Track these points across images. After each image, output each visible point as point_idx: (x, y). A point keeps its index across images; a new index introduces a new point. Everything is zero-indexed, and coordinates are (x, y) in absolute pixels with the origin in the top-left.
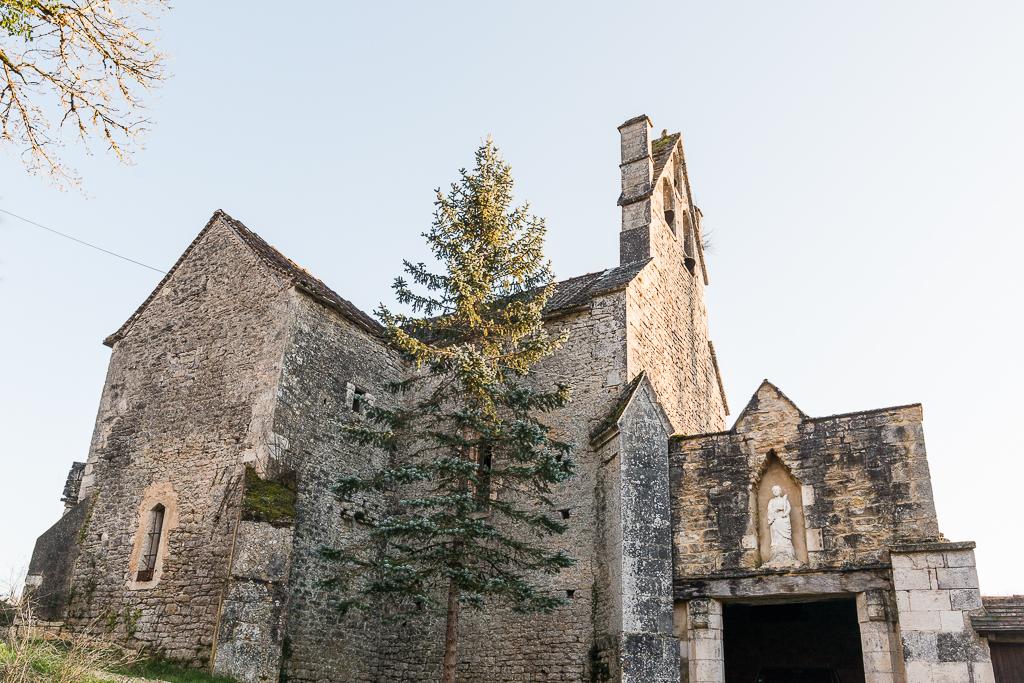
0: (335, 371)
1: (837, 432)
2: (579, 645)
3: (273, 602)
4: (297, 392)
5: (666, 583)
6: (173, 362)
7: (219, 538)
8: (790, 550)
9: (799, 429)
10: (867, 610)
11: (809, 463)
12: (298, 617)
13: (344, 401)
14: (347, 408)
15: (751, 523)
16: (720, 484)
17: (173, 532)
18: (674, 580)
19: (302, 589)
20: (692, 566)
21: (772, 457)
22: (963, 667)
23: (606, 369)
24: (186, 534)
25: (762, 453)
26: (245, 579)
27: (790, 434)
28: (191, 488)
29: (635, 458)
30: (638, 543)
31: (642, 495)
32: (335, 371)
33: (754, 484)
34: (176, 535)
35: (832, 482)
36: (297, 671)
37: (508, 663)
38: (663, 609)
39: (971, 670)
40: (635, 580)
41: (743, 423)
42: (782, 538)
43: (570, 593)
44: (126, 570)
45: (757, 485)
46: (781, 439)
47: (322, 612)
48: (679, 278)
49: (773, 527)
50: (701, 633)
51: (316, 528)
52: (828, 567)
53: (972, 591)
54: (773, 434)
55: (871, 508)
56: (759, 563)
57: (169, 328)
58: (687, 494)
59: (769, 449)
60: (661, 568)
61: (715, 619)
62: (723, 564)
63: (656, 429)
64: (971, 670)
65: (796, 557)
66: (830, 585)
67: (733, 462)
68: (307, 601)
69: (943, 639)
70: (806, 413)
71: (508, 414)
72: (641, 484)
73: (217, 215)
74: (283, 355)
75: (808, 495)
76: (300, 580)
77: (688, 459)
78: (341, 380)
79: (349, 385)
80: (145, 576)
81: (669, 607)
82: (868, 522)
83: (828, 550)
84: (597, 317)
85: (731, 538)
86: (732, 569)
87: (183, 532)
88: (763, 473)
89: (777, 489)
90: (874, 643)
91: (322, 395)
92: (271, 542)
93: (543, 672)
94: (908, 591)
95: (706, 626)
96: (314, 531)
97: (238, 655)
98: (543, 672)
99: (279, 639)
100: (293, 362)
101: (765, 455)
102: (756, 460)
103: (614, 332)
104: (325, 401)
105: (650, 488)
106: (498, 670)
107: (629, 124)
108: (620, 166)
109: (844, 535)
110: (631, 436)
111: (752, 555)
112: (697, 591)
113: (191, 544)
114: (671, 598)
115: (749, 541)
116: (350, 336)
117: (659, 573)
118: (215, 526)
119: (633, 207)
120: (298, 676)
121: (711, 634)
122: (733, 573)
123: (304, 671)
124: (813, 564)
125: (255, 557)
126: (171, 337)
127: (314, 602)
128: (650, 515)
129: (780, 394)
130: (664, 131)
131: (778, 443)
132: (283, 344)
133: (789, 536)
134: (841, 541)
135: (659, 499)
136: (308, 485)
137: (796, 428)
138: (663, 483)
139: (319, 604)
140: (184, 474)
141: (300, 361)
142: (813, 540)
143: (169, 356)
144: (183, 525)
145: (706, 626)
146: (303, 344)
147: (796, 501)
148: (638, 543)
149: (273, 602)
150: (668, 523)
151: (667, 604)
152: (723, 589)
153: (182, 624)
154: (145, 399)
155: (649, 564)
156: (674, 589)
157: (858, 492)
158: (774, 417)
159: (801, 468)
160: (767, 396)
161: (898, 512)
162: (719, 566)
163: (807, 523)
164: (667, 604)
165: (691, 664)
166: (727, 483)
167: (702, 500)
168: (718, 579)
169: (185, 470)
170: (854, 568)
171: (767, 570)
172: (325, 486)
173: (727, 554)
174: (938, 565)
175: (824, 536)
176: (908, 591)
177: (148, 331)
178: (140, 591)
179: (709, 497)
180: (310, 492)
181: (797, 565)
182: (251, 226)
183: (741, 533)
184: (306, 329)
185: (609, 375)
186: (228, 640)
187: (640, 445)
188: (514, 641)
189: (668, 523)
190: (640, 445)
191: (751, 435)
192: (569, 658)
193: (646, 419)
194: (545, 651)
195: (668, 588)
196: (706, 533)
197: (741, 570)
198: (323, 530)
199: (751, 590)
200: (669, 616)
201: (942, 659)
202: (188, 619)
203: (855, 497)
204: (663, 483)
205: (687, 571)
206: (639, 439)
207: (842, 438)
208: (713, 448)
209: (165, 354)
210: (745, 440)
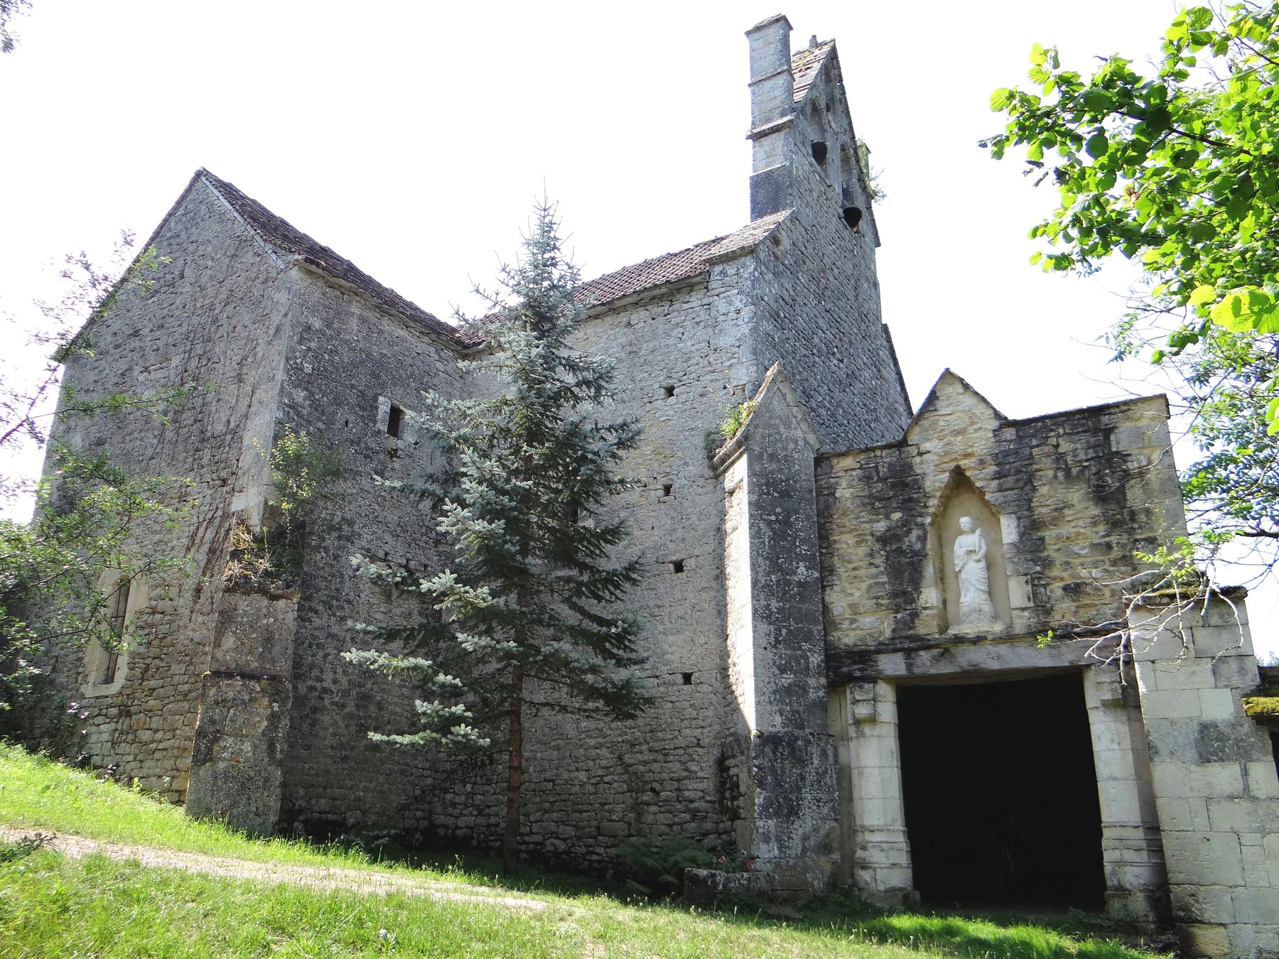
0: (362, 380)
2: (700, 751)
3: (270, 706)
4: (305, 412)
5: (816, 659)
6: (141, 378)
7: (200, 619)
8: (987, 607)
9: (995, 436)
10: (1096, 693)
12: (313, 725)
13: (375, 422)
14: (379, 432)
15: (929, 570)
16: (887, 517)
17: (141, 613)
18: (826, 656)
19: (318, 685)
20: (852, 634)
21: (958, 473)
22: (1234, 769)
23: (728, 363)
24: (158, 616)
26: (230, 675)
27: (982, 441)
28: (164, 551)
29: (767, 484)
30: (775, 604)
31: (778, 536)
32: (362, 380)
34: (145, 617)
35: (1043, 510)
36: (314, 801)
37: (606, 779)
38: (812, 695)
39: (1245, 773)
40: (771, 655)
42: (976, 589)
43: (687, 678)
44: (81, 670)
46: (970, 451)
47: (350, 716)
48: (836, 236)
49: (963, 575)
50: (867, 729)
51: (338, 600)
53: (1244, 656)
54: (959, 443)
56: (944, 628)
57: (136, 334)
58: (841, 533)
59: (953, 465)
60: (808, 637)
61: (888, 711)
62: (894, 631)
63: (796, 442)
64: (1245, 773)
65: (995, 617)
66: (1041, 656)
68: (327, 702)
69: (1206, 729)
72: (777, 521)
73: (198, 175)
74: (283, 360)
75: (1009, 530)
76: (315, 672)
78: (370, 393)
79: (381, 399)
80: (109, 679)
81: (821, 693)
82: (1095, 565)
83: (1042, 607)
84: (716, 292)
85: (905, 593)
86: (907, 637)
87: (154, 613)
88: (946, 503)
89: (965, 521)
90: (1108, 740)
91: (342, 414)
92: (265, 621)
93: (653, 790)
94: (1153, 662)
95: (873, 720)
96: (335, 603)
97: (220, 783)
98: (653, 790)
99: (279, 756)
100: (299, 369)
101: (947, 474)
102: (935, 480)
103: (738, 312)
104: (347, 423)
105: (790, 525)
106: (592, 789)
107: (758, 29)
108: (750, 85)
109: (1062, 584)
110: (761, 454)
112: (860, 670)
113: (165, 628)
114: (823, 680)
115: (929, 596)
116: (381, 332)
117: (805, 646)
118: (195, 603)
119: (766, 141)
120: (316, 809)
121: (879, 730)
122: (908, 643)
123: (323, 801)
124: (1020, 626)
125: (243, 644)
126: (137, 344)
127: (336, 704)
128: (791, 564)
129: (966, 387)
130: (814, 37)
131: (967, 455)
132: (281, 345)
133: (984, 587)
134: (1060, 592)
135: (803, 541)
136: (324, 540)
138: (808, 517)
139: (344, 706)
140: (156, 532)
141: (308, 368)
142: (1017, 593)
143: (137, 369)
144: (154, 603)
145: (873, 720)
146: (313, 345)
147: (993, 538)
148: (775, 604)
149: (270, 706)
150: (816, 575)
151: (818, 688)
152: (892, 664)
153: (152, 742)
154: (106, 434)
155: (790, 632)
156: (828, 668)
157: (1081, 522)
158: (959, 421)
159: (1000, 491)
162: (888, 634)
163: (1010, 569)
164: (818, 688)
165: (855, 772)
166: (897, 516)
167: (863, 541)
169: (157, 527)
172: (348, 539)
173: (899, 616)
174: (1194, 623)
175: (1033, 586)
176: (1153, 662)
177: (109, 338)
178: (97, 698)
179: (872, 535)
180: (326, 550)
181: (998, 628)
182: (250, 190)
184: (317, 324)
185: (733, 371)
186: (205, 761)
187: (774, 466)
188: (612, 747)
189: (816, 575)
190: (774, 466)
192: (687, 770)
193: (782, 430)
194: (655, 761)
195: (819, 666)
196: (870, 587)
197: (918, 638)
198: (349, 602)
199: (926, 663)
200: (822, 706)
201: (1204, 759)
202: (159, 735)
205: (846, 640)
206: (772, 457)
207: (1057, 446)
208: (876, 467)
209: (130, 369)
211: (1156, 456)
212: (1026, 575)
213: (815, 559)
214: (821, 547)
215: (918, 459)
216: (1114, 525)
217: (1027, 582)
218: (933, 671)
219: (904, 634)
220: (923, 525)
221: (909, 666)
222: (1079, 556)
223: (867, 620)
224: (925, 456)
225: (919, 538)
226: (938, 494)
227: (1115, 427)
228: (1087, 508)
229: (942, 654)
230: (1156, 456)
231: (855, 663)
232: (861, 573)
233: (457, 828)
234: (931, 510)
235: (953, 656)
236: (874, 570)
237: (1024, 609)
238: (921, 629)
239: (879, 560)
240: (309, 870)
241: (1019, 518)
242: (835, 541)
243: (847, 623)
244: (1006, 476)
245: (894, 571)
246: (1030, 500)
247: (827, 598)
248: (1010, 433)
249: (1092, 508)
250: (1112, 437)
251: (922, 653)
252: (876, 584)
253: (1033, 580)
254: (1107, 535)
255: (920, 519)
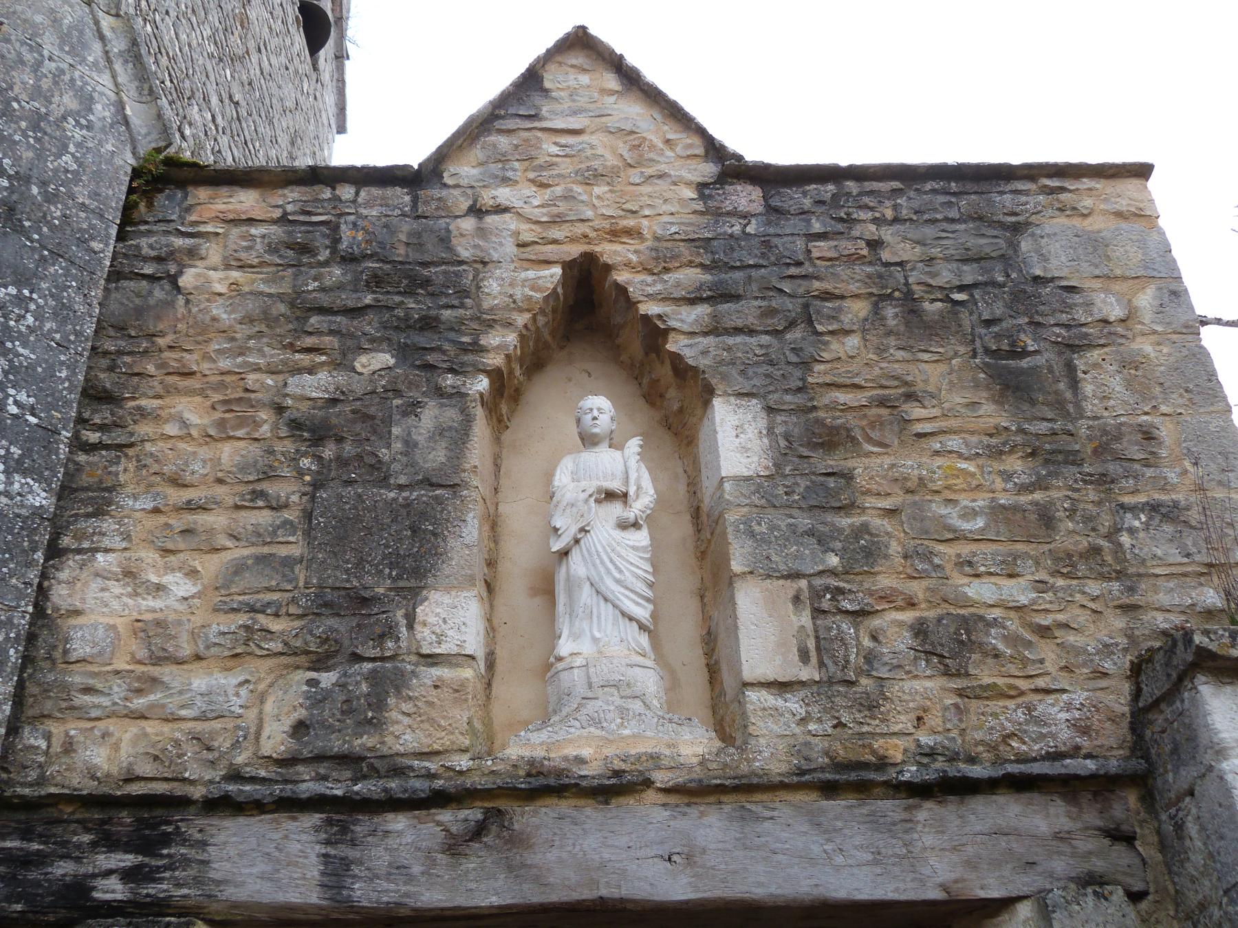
1: (849, 221)
11: (746, 312)
20: (127, 733)
25: (548, 263)
27: (668, 200)
33: (496, 375)
41: (477, 153)
45: (506, 394)
46: (630, 222)
49: (577, 565)
52: (839, 766)
55: (1015, 508)
59: (575, 251)
62: (300, 728)
63: (87, 102)
67: (416, 284)
70: (733, 143)
71: (170, 522)
77: (214, 252)
85: (363, 600)
86: (346, 760)
88: (536, 358)
101: (557, 270)
109: (908, 616)
111: (459, 689)
112: (128, 875)
115: (451, 618)
129: (630, 79)
131: (615, 234)
134: (900, 642)
137: (690, 193)
150: (40, 498)
157: (954, 443)
160: (573, 82)
161: (1132, 531)
162: (275, 739)
166: (379, 360)
168: (257, 807)
170: (976, 771)
171: (535, 769)
173: (328, 679)
175: (818, 612)
179: (280, 409)
183: (415, 571)
189: (40, 498)
191: (504, 194)
196: (239, 568)
203: (948, 461)
204: (63, 313)
210: (477, 211)
211: (1146, 300)
212: (794, 576)
213: (49, 448)
214: (81, 421)
215: (468, 224)
216: (1052, 456)
217: (797, 599)
218: (432, 896)
219: (337, 745)
220: (460, 394)
221: (336, 872)
222: (958, 537)
223: (199, 682)
224: (491, 220)
225: (440, 431)
226: (521, 319)
227: (1028, 224)
228: (974, 405)
229: (478, 832)
230: (1146, 300)
231: (110, 842)
232: (217, 520)
233: (15, 663)
234: (495, 360)
235: (517, 841)
236: (264, 518)
237: (781, 687)
238: (404, 734)
239: (286, 489)
240: (850, 396)
241: (770, 410)
242: (142, 413)
243: (118, 689)
244: (735, 298)
245: (330, 529)
246: (806, 365)
247: (60, 595)
248: (746, 197)
249: (988, 408)
250: (1025, 245)
251: (399, 822)
252: (261, 559)
253: (817, 595)
254: (1039, 484)
255: (450, 380)
